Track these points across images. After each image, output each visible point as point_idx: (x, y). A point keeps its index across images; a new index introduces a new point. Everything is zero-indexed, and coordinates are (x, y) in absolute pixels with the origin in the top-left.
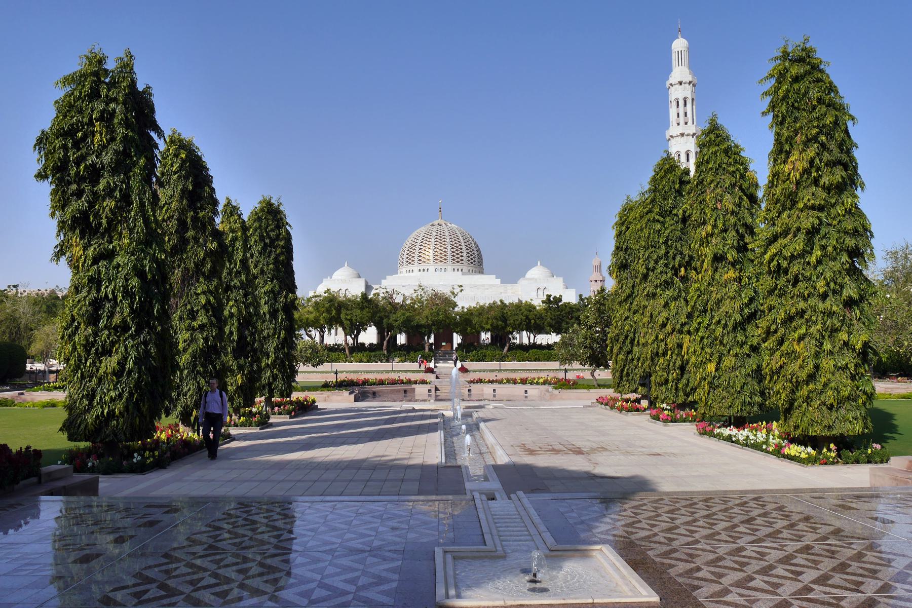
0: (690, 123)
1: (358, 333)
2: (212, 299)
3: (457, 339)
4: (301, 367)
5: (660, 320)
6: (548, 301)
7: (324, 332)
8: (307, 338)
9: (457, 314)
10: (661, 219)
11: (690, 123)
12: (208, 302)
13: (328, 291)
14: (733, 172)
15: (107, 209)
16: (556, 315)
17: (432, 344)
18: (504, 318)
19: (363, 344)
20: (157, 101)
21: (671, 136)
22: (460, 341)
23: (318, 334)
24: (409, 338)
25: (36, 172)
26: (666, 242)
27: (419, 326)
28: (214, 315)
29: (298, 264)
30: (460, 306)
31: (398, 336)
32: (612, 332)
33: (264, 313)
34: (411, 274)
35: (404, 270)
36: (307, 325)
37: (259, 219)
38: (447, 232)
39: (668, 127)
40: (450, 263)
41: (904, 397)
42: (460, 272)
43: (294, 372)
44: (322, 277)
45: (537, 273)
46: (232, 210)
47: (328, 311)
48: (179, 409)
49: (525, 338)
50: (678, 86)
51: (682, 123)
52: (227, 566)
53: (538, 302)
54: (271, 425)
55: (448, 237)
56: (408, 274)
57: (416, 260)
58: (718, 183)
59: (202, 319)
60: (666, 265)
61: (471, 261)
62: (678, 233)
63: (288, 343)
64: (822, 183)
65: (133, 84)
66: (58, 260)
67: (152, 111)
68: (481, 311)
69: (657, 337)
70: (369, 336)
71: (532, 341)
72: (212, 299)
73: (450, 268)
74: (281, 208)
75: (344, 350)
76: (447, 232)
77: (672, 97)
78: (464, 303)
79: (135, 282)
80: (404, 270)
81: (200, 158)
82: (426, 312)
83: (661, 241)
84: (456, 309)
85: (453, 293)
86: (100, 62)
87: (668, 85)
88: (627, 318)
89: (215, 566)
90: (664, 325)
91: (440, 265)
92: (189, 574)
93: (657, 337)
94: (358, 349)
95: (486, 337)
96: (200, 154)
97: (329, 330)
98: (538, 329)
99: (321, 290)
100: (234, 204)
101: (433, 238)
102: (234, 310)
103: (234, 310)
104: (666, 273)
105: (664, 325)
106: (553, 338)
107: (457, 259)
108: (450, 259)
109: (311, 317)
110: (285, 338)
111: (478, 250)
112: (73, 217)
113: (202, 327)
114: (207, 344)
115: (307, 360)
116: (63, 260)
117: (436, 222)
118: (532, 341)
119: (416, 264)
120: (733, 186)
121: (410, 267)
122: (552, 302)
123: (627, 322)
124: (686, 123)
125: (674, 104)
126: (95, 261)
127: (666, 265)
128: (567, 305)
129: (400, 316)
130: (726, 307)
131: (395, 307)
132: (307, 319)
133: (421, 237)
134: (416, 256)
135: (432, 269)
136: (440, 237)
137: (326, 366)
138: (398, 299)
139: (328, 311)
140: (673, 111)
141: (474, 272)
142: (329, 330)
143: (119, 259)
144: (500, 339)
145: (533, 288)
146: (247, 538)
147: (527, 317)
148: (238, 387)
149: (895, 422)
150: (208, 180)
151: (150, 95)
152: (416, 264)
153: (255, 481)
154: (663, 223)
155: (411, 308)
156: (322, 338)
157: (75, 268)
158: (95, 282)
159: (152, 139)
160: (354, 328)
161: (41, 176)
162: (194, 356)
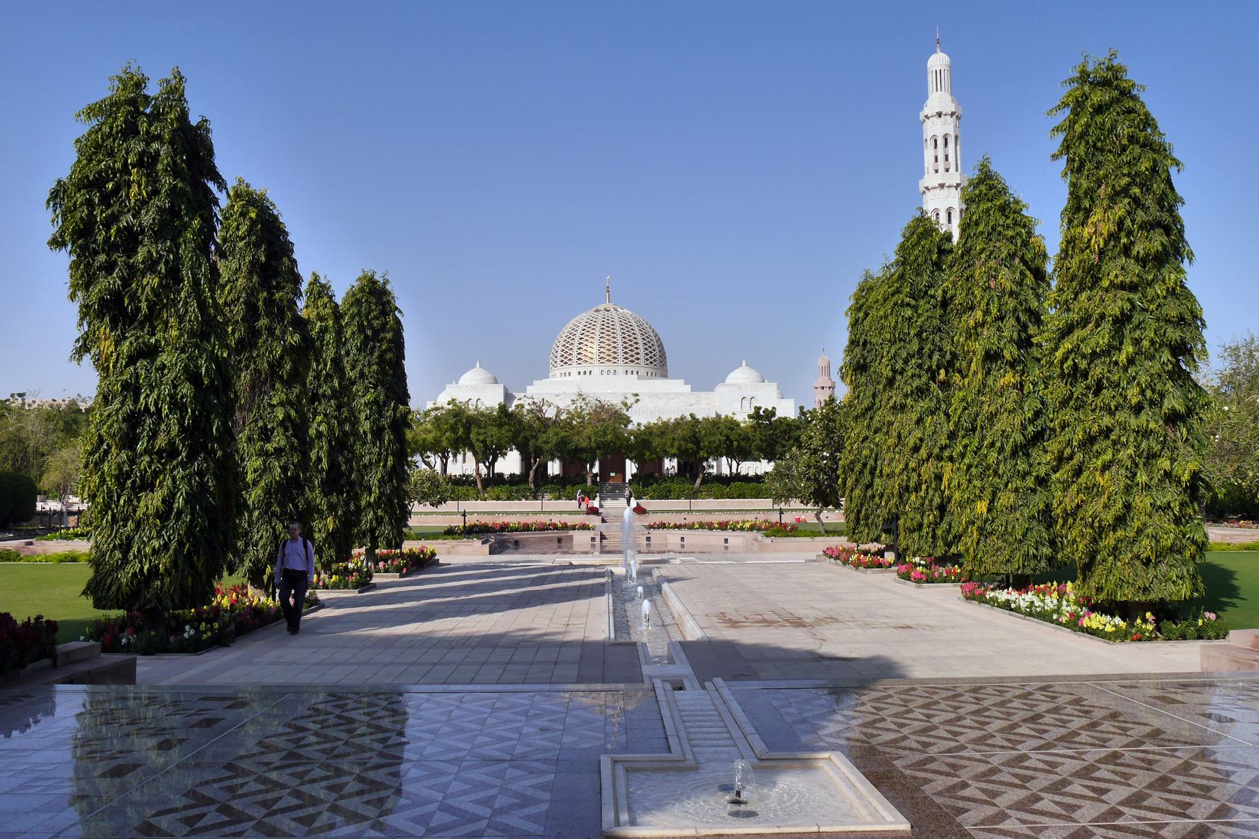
0: (952, 169)
1: (495, 460)
2: (293, 413)
3: (631, 468)
4: (416, 507)
5: (911, 441)
6: (756, 415)
7: (447, 459)
8: (424, 466)
9: (631, 433)
10: (913, 302)
11: (952, 169)
12: (287, 416)
13: (453, 401)
14: (1012, 237)
15: (148, 289)
16: (768, 435)
17: (596, 475)
18: (696, 439)
19: (501, 475)
20: (216, 139)
21: (927, 188)
22: (635, 471)
23: (439, 461)
24: (564, 467)
25: (49, 238)
26: (919, 335)
27: (578, 450)
28: (295, 435)
29: (412, 365)
30: (635, 422)
31: (550, 463)
32: (844, 459)
33: (365, 432)
34: (568, 378)
35: (558, 373)
36: (423, 448)
37: (358, 302)
38: (617, 320)
39: (922, 175)
40: (621, 362)
41: (1248, 548)
42: (635, 375)
43: (406, 514)
44: (444, 382)
45: (741, 376)
46: (320, 290)
47: (453, 429)
48: (247, 564)
49: (724, 466)
50: (936, 119)
51: (941, 169)
52: (313, 781)
53: (742, 417)
54: (375, 587)
55: (618, 327)
56: (563, 378)
57: (575, 359)
58: (991, 253)
59: (279, 440)
60: (920, 366)
61: (650, 361)
62: (936, 322)
63: (398, 473)
64: (1134, 252)
65: (183, 116)
66: (80, 359)
67: (210, 153)
68: (664, 429)
69: (907, 465)
70: (510, 464)
71: (734, 471)
72: (293, 413)
73: (621, 370)
74: (388, 287)
75: (475, 482)
76: (617, 320)
77: (928, 134)
78: (641, 418)
79: (186, 389)
80: (558, 373)
81: (276, 218)
82: (588, 431)
83: (912, 332)
84: (630, 427)
85: (625, 405)
86: (139, 85)
87: (922, 117)
88: (866, 438)
89: (297, 782)
90: (916, 449)
91: (607, 366)
92: (260, 792)
93: (907, 465)
94: (495, 482)
95: (670, 465)
96: (275, 212)
97: (455, 456)
98: (743, 454)
99: (443, 400)
100: (323, 281)
101: (598, 329)
102: (323, 428)
103: (323, 428)
104: (920, 376)
105: (916, 449)
106: (763, 467)
107: (631, 358)
108: (621, 358)
109: (430, 437)
110: (393, 467)
111: (660, 345)
112: (101, 299)
113: (279, 452)
114: (286, 475)
115: (424, 497)
116: (87, 358)
117: (602, 307)
118: (734, 471)
119: (575, 364)
120: (1012, 256)
121: (566, 369)
122: (762, 417)
123: (866, 444)
124: (947, 170)
125: (930, 144)
126: (132, 360)
127: (920, 366)
128: (783, 421)
129: (552, 436)
130: (1003, 423)
131: (545, 423)
132: (424, 440)
133: (582, 327)
134: (575, 354)
135: (596, 371)
136: (607, 326)
137: (450, 506)
138: (550, 413)
139: (453, 429)
140: (929, 153)
141: (654, 375)
142: (455, 456)
143: (164, 358)
144: (691, 468)
145: (736, 397)
146: (340, 743)
147: (728, 438)
148: (329, 534)
149: (1235, 583)
150: (287, 249)
151: (208, 130)
152: (575, 364)
153: (352, 664)
154: (915, 308)
155: (568, 424)
156: (445, 466)
157: (104, 369)
158: (132, 389)
159: (210, 192)
160: (489, 453)
161: (57, 243)
162: (267, 491)
